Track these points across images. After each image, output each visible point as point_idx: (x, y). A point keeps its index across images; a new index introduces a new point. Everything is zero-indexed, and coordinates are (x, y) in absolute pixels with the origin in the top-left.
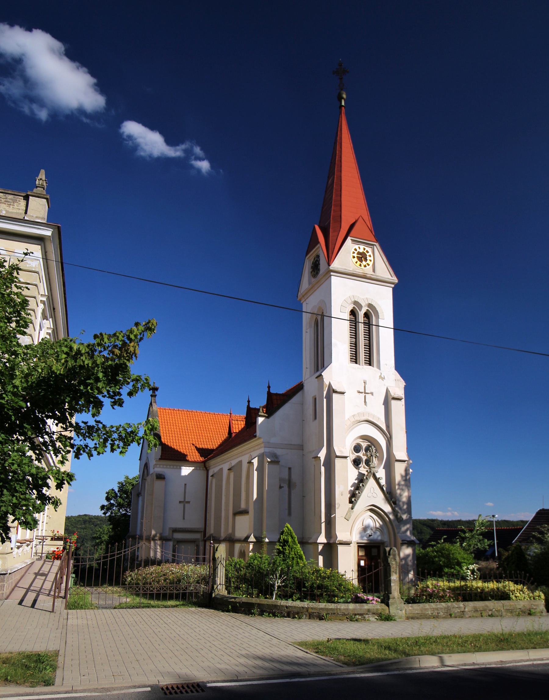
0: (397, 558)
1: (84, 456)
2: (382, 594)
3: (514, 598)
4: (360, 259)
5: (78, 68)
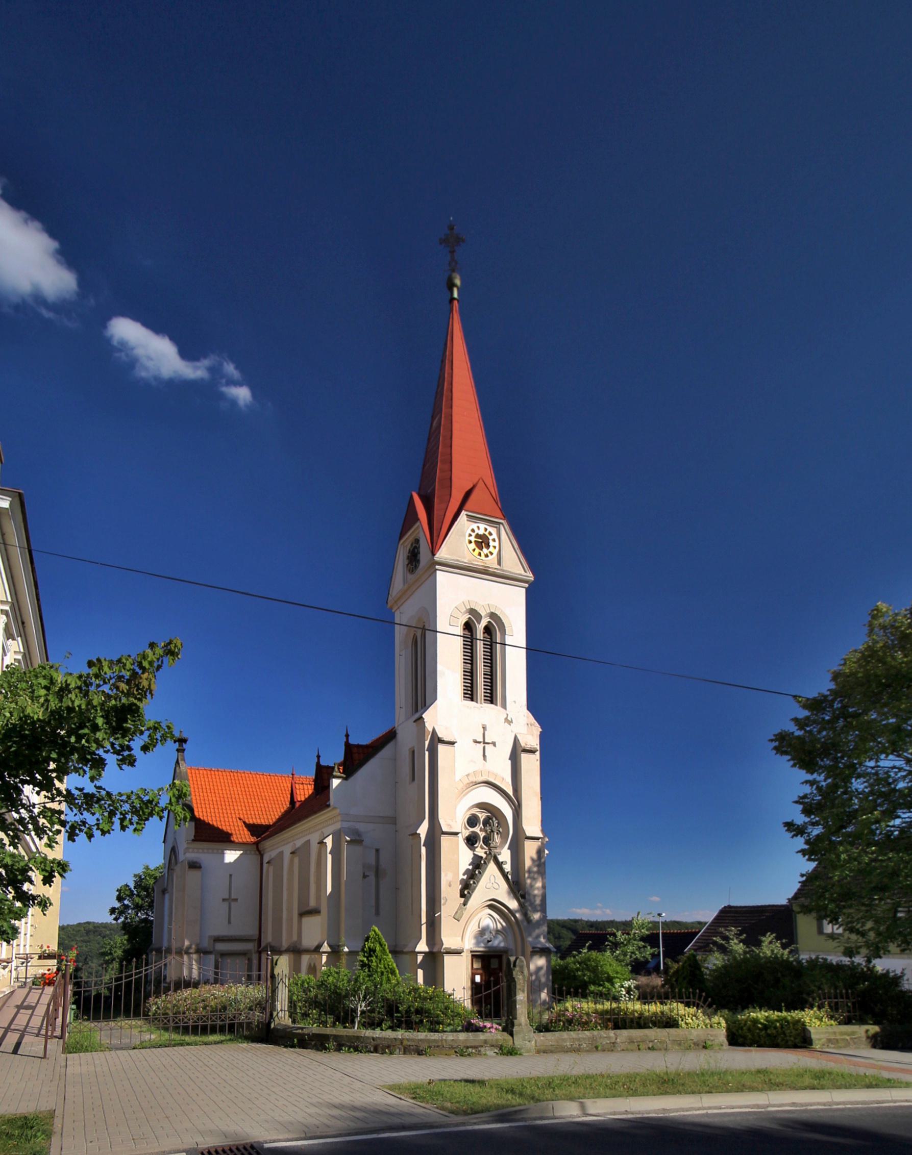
0: (526, 972)
1: (82, 837)
2: (504, 1019)
3: (684, 1025)
4: (479, 545)
5: (26, 222)
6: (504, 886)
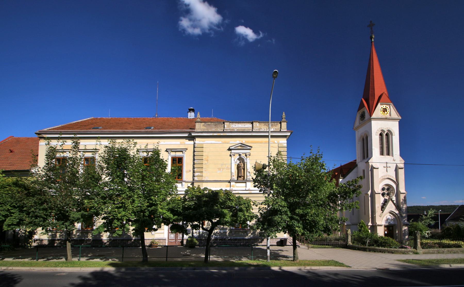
4: (384, 111)
6: (394, 207)
